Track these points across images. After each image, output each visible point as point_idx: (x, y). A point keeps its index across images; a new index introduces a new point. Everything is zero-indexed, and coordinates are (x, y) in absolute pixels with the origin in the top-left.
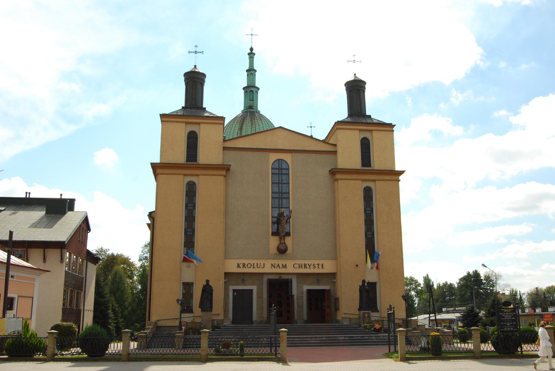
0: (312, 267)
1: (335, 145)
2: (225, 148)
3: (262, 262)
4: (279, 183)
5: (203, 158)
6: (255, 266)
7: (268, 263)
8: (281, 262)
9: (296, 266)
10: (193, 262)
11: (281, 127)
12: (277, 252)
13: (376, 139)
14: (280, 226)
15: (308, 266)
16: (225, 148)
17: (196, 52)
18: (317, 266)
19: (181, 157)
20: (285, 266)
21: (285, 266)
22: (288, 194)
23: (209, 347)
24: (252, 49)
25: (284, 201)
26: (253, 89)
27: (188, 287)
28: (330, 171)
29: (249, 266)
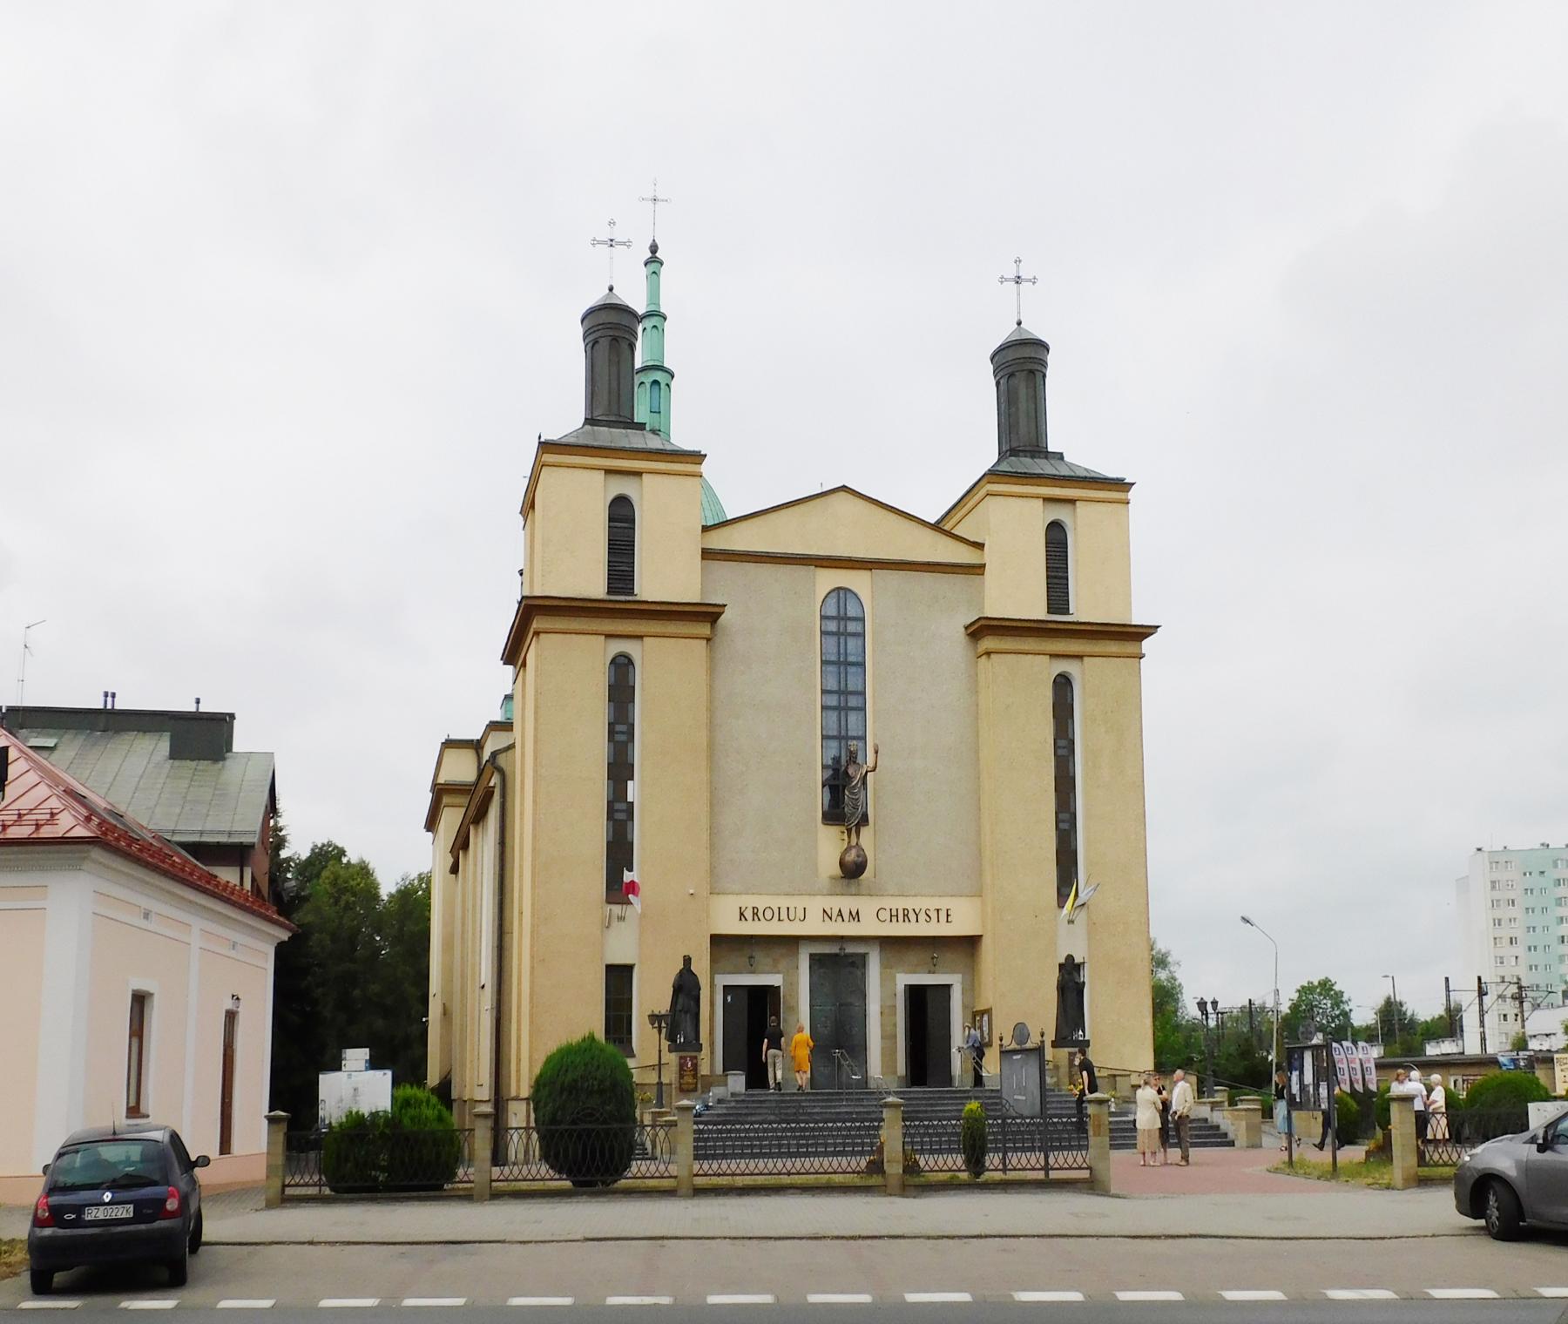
0: (922, 917)
1: (979, 546)
2: (707, 554)
3: (797, 903)
4: (838, 663)
5: (650, 585)
6: (784, 915)
7: (816, 905)
8: (847, 903)
9: (885, 915)
10: (1061, 905)
11: (844, 488)
12: (837, 871)
13: (1086, 524)
14: (842, 799)
15: (912, 916)
16: (707, 554)
17: (611, 243)
18: (933, 915)
19: (587, 578)
20: (855, 916)
21: (855, 916)
22: (860, 698)
23: (696, 1157)
24: (654, 249)
25: (853, 717)
26: (658, 376)
27: (619, 978)
28: (966, 628)
29: (769, 914)
